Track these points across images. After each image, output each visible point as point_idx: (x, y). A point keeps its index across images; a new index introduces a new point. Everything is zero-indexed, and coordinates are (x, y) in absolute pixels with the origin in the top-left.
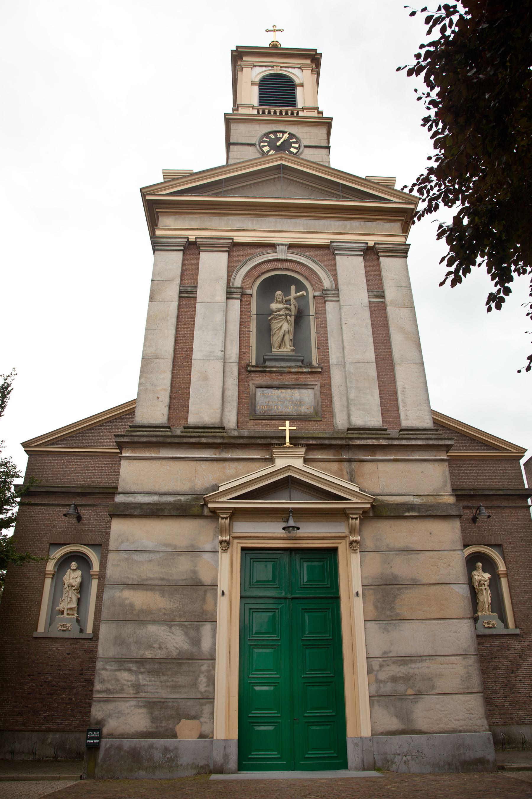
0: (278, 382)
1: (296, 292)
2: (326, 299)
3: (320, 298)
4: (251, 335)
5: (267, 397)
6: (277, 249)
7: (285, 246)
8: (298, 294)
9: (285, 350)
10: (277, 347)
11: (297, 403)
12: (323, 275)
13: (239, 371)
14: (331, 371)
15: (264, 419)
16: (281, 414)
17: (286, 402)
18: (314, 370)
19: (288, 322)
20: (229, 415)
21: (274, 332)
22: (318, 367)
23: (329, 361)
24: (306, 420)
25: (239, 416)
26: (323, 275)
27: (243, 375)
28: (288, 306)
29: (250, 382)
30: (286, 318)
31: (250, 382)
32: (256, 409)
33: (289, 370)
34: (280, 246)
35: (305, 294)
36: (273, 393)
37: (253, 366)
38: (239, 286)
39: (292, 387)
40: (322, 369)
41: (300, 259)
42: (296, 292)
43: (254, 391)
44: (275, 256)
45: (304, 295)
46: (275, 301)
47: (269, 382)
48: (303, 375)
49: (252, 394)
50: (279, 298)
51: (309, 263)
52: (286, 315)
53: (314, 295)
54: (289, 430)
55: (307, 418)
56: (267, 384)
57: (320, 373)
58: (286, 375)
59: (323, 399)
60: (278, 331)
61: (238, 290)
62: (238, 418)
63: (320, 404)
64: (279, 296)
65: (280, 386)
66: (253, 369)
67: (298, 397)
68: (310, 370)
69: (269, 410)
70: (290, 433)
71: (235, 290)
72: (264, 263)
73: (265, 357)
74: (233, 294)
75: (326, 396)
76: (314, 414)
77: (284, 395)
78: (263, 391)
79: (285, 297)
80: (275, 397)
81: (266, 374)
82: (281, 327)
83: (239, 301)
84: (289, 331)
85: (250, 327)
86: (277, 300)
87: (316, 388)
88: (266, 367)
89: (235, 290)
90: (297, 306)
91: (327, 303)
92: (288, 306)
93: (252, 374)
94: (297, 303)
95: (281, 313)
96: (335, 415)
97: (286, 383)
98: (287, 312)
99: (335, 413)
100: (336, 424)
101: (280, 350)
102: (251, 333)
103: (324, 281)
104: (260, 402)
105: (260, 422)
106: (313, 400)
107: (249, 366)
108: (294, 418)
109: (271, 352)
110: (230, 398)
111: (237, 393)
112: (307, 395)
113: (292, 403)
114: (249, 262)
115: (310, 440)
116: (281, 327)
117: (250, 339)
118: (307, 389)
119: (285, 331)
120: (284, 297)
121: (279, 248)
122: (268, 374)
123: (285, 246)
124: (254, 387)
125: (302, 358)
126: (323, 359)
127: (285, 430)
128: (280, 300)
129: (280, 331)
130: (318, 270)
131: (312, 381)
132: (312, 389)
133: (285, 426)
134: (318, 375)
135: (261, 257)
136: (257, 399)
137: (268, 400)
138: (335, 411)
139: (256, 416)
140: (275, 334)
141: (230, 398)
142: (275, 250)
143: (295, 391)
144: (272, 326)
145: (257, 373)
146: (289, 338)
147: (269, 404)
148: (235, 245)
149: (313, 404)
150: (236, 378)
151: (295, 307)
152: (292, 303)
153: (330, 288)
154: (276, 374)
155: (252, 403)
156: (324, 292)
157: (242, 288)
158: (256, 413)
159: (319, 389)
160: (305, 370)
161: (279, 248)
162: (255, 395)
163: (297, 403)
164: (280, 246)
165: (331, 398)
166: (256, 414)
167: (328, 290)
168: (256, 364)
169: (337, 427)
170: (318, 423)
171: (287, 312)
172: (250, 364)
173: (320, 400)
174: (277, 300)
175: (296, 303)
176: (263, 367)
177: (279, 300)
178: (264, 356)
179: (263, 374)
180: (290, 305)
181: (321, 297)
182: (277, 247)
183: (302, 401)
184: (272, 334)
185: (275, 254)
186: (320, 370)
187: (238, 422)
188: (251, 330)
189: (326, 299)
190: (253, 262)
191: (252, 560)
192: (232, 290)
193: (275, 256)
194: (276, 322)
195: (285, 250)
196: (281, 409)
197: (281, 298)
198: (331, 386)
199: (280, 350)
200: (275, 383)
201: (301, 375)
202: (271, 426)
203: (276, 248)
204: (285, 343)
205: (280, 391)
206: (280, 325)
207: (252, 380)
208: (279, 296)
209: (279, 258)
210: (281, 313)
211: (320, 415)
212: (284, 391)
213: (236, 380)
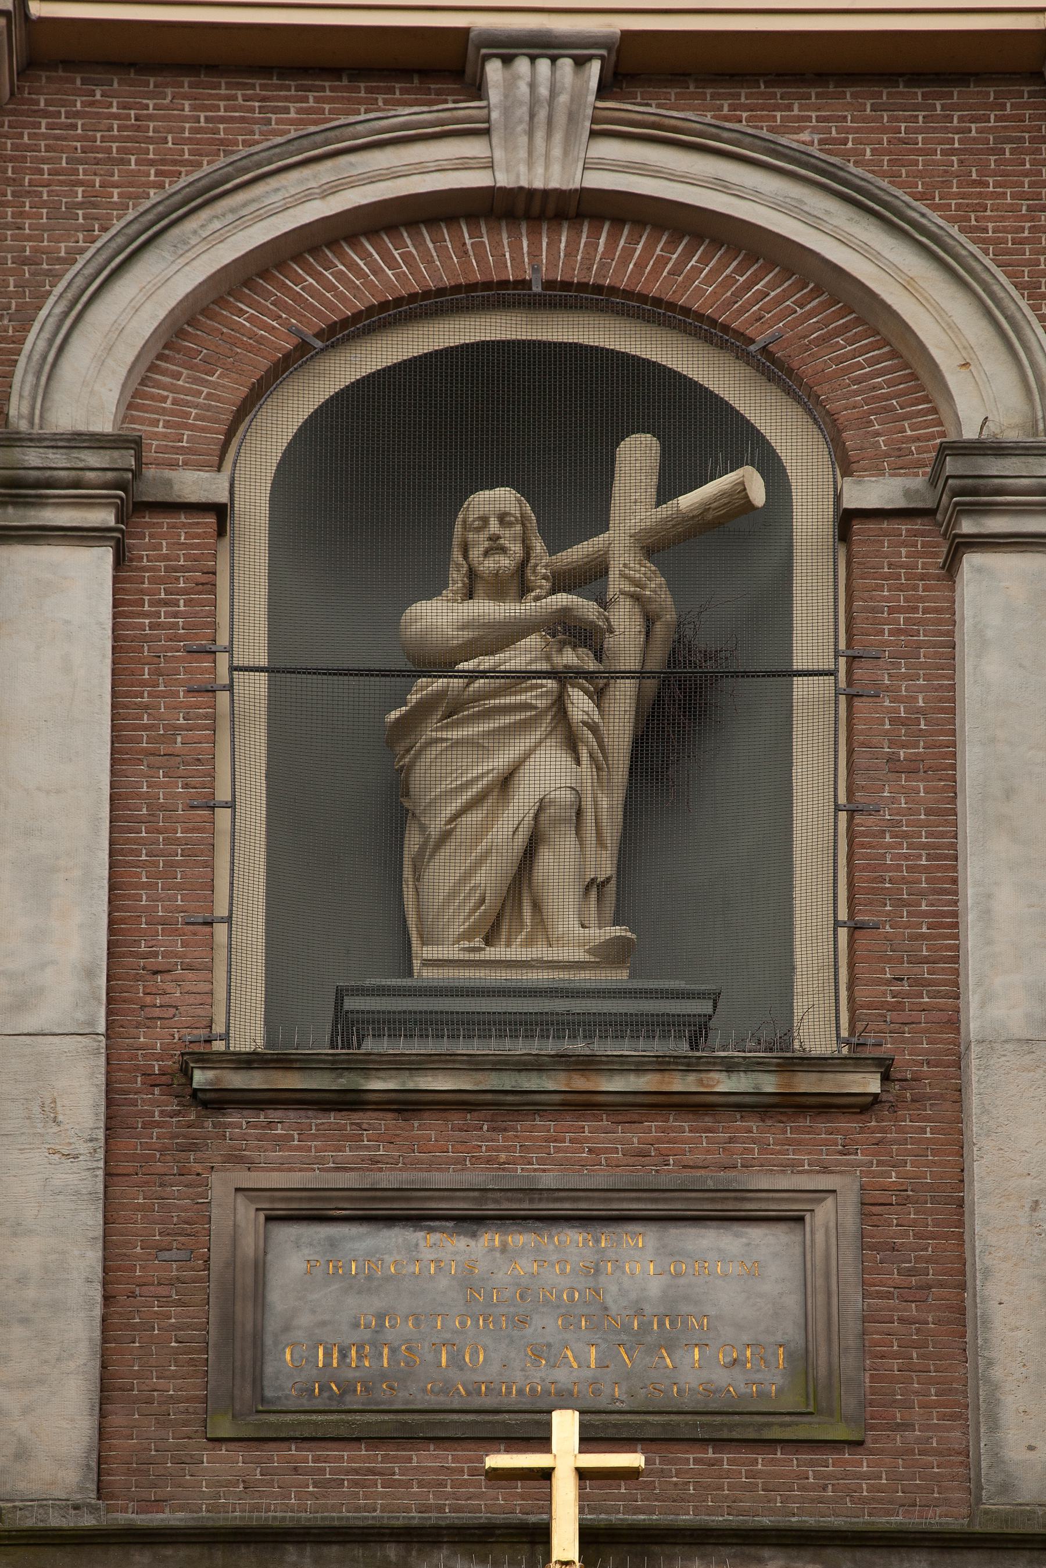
0: (475, 1177)
1: (666, 492)
2: (967, 526)
3: (904, 527)
4: (221, 955)
5: (369, 1284)
6: (495, 95)
7: (580, 62)
8: (688, 501)
9: (540, 952)
10: (467, 935)
11: (645, 1328)
12: (951, 328)
13: (110, 1103)
14: (974, 1102)
15: (344, 1432)
16: (489, 1402)
17: (537, 1321)
18: (806, 1083)
19: (572, 744)
20: (26, 1411)
21: (436, 825)
22: (855, 1062)
23: (953, 1023)
24: (720, 1443)
25: (117, 1420)
26: (951, 328)
27: (147, 1125)
28: (585, 607)
29: (214, 1178)
30: (560, 706)
31: (214, 1178)
32: (269, 1370)
33: (580, 1083)
34: (522, 65)
35: (758, 494)
36: (427, 1254)
37: (248, 1061)
38: (104, 425)
39: (598, 1207)
40: (886, 1078)
41: (721, 186)
42: (666, 492)
43: (248, 1245)
44: (464, 165)
45: (748, 506)
46: (457, 578)
47: (387, 1179)
48: (708, 1121)
49: (232, 1264)
50: (496, 547)
51: (814, 223)
52: (564, 677)
53: (850, 502)
54: (582, 1474)
55: (732, 1427)
56: (374, 1192)
57: (867, 1105)
58: (543, 1126)
59: (880, 1295)
60: (475, 817)
61: (93, 459)
62: (102, 1433)
63: (853, 1326)
64: (494, 526)
65: (490, 1207)
66: (237, 1080)
67: (655, 1287)
68: (769, 1084)
69: (383, 1376)
70: (584, 1501)
71: (57, 459)
72: (352, 239)
73: (351, 1004)
74: (40, 502)
75: (910, 1272)
76: (792, 1401)
77: (525, 1266)
78: (332, 1243)
79: (553, 549)
80: (443, 1283)
81: (357, 1117)
82: (506, 782)
83: (104, 556)
84: (579, 813)
85: (212, 775)
86: (472, 574)
87: (823, 1213)
88: (368, 1065)
89: (57, 459)
90: (670, 616)
91: (971, 561)
92: (585, 607)
93: (236, 1120)
94: (672, 586)
95: (514, 659)
96: (994, 1403)
97: (549, 1180)
98: (569, 658)
99: (995, 1387)
100: (998, 1460)
101: (491, 953)
102: (223, 816)
103: (954, 380)
104: (305, 1320)
105: (307, 1456)
106: (792, 1302)
107: (206, 1060)
108: (606, 1425)
109: (405, 965)
110: (31, 1293)
111: (94, 1256)
112: (733, 1269)
113: (594, 1328)
114: (191, 224)
115: (766, 1553)
116: (506, 782)
117: (210, 865)
118: (737, 1227)
119: (542, 806)
120: (538, 545)
121: (510, 86)
122: (384, 1122)
123: (580, 62)
124: (247, 1215)
125: (704, 1007)
126: (897, 1007)
127: (546, 1474)
128: (505, 562)
129: (492, 817)
130: (908, 286)
131: (794, 1167)
132: (780, 1229)
133: (549, 1451)
134: (847, 1124)
135: (325, 172)
136: (278, 1298)
137: (377, 1303)
138: (997, 1373)
139: (272, 1418)
140: (445, 836)
141: (31, 1293)
142: (469, 108)
143: (628, 1241)
144: (418, 778)
145: (275, 1115)
146: (581, 870)
147: (390, 1335)
148: (51, 65)
149: (789, 1330)
150: (83, 1148)
151: (649, 620)
152: (615, 584)
153: (1012, 435)
154: (456, 1119)
155: (228, 1322)
156: (951, 466)
157: (136, 444)
158: (263, 1400)
159: (850, 1220)
160: (724, 1084)
161: (510, 86)
162: (260, 1269)
163: (645, 1328)
164: (522, 65)
165: (963, 1286)
166: (262, 1404)
167: (998, 449)
168: (270, 1042)
169: (1005, 1488)
170: (831, 1463)
171: (569, 658)
172: (219, 1046)
173: (855, 1302)
174: (472, 574)
175: (656, 586)
176: (335, 1066)
177: (489, 565)
178: (340, 995)
179: (332, 1118)
180: (604, 603)
181: (918, 525)
182: (494, 70)
183: (684, 1308)
184: (413, 842)
185: (472, 148)
186: (872, 1084)
187: (100, 1461)
188: (223, 794)
189: (967, 526)
190: (241, 223)
191: (262, 1216)
192: (33, 457)
193: (464, 165)
194: (458, 743)
195: (577, 98)
196: (494, 1369)
197: (516, 549)
198: (961, 1204)
199: (491, 953)
200: (441, 1179)
201: (683, 1127)
202: (408, 1484)
203: (477, 90)
204: (537, 907)
205: (490, 1239)
206: (501, 760)
207: (236, 1159)
208: (494, 526)
209: (504, 180)
210: (514, 659)
211: (849, 1403)
212: (520, 1239)
213: (83, 1163)
